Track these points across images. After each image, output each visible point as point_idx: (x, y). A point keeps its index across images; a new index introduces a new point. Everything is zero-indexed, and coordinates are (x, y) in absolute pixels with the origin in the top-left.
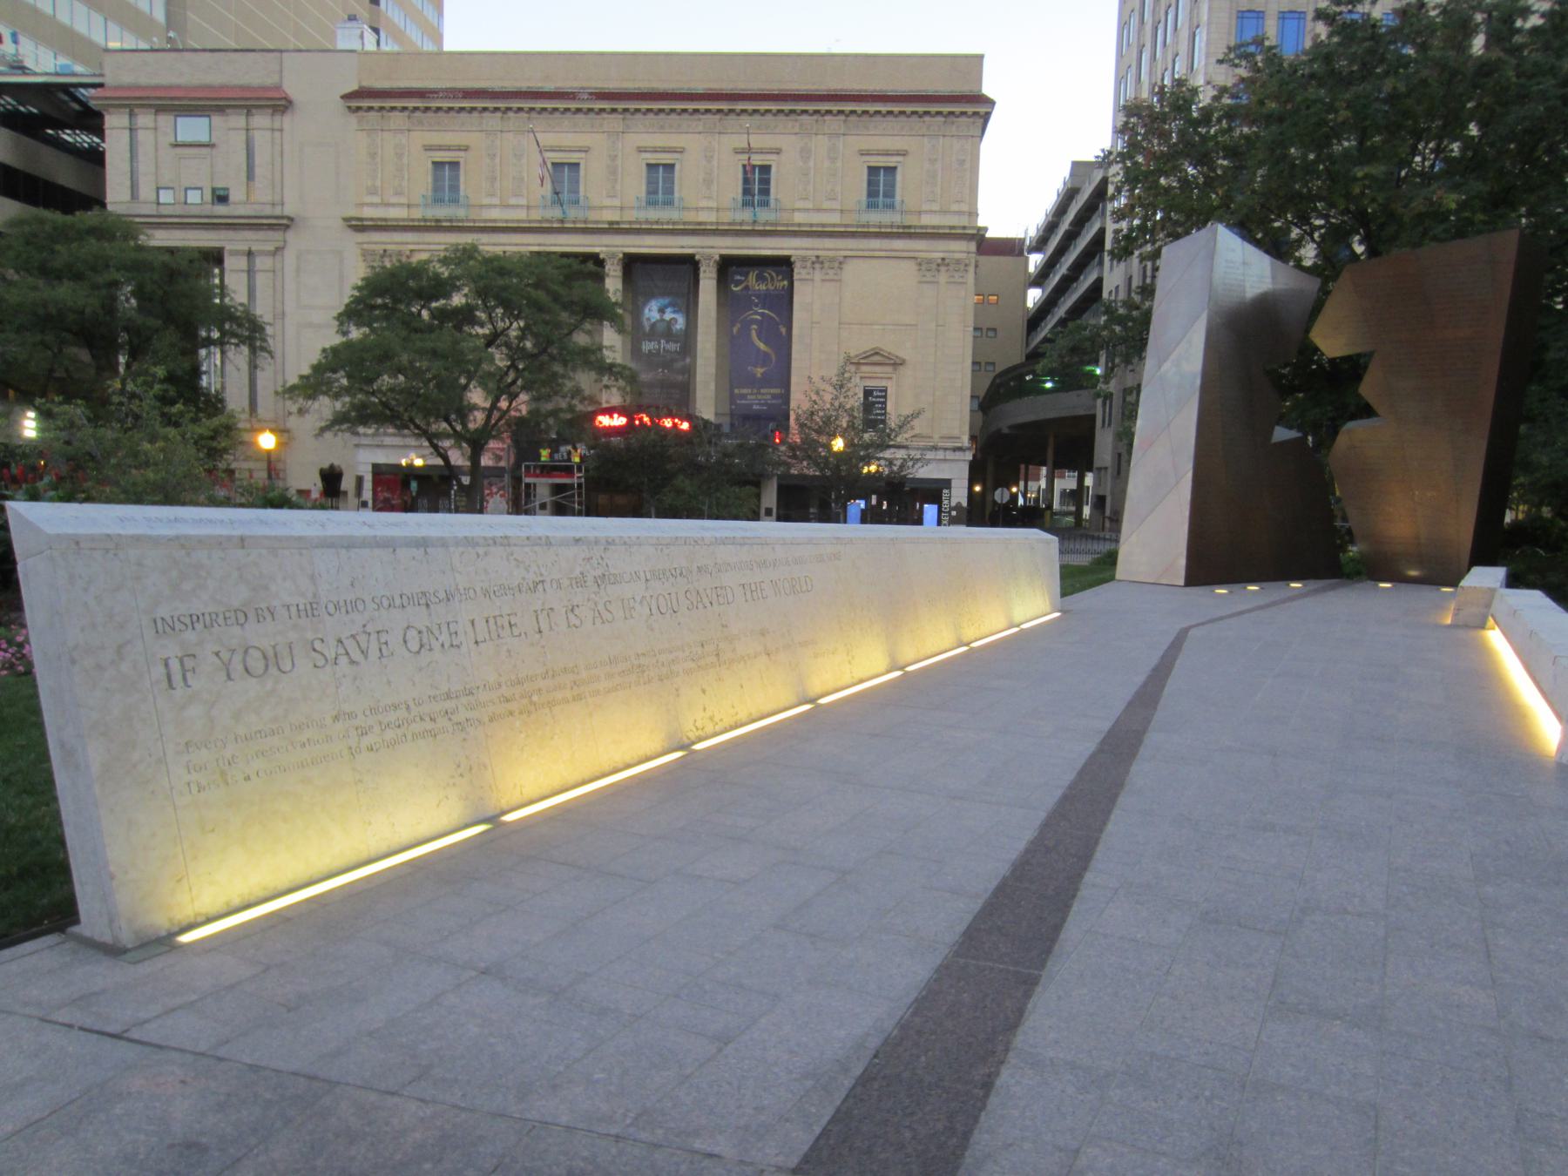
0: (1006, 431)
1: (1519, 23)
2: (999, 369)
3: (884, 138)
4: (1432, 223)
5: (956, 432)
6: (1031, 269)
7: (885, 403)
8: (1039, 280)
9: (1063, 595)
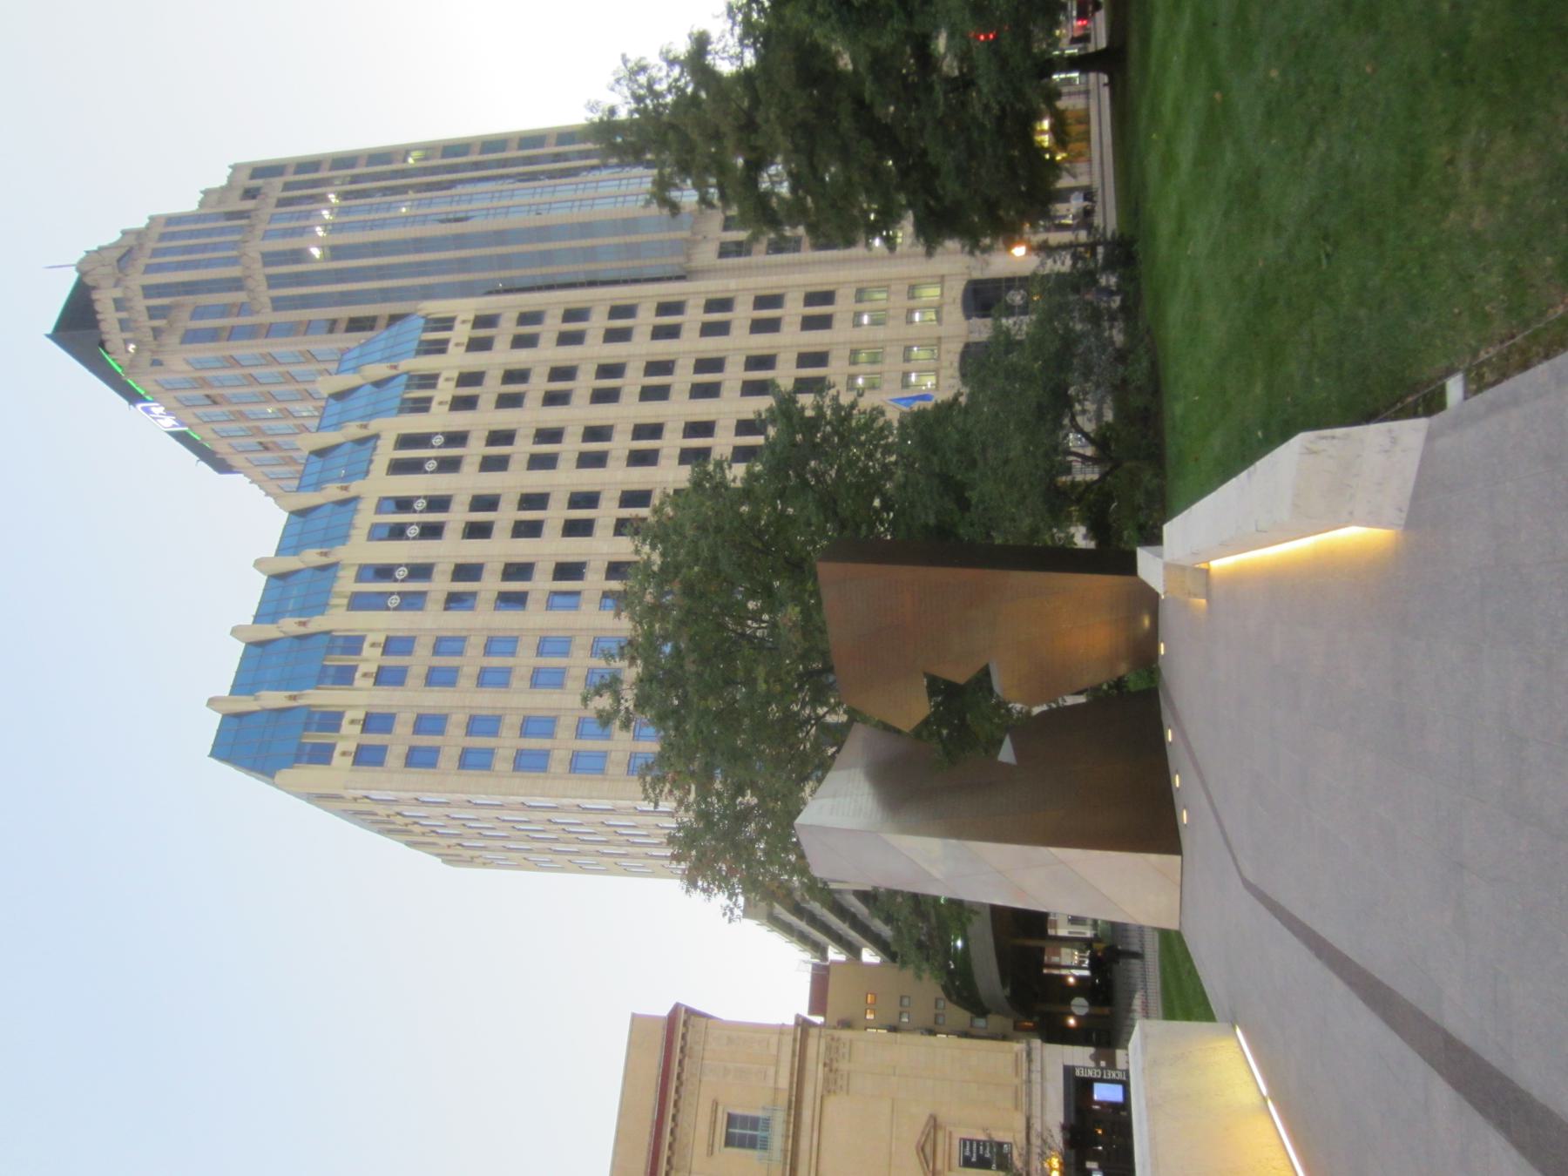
0: (1007, 991)
1: (655, 568)
2: (941, 994)
3: (699, 1126)
4: (811, 626)
5: (1010, 1058)
6: (842, 957)
7: (978, 1142)
8: (853, 950)
9: (1208, 1016)
